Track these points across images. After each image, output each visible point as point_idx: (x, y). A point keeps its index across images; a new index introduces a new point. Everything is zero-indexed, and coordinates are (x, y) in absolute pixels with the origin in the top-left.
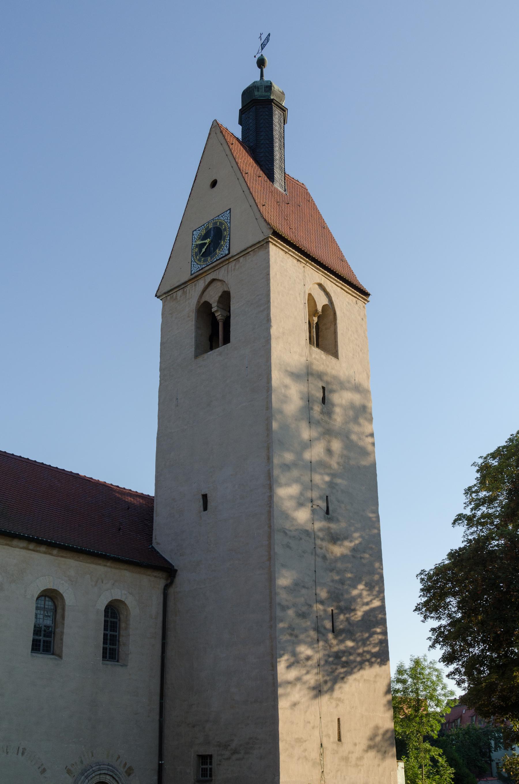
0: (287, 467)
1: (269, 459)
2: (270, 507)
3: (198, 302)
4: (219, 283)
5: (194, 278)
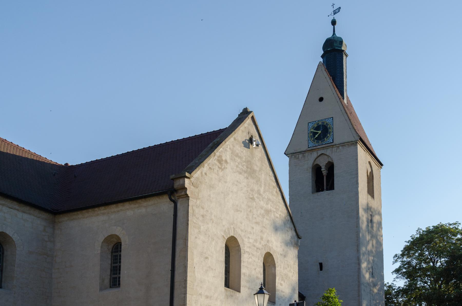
0: (364, 254)
1: (358, 251)
2: (359, 273)
3: (313, 163)
4: (326, 157)
5: (311, 151)
